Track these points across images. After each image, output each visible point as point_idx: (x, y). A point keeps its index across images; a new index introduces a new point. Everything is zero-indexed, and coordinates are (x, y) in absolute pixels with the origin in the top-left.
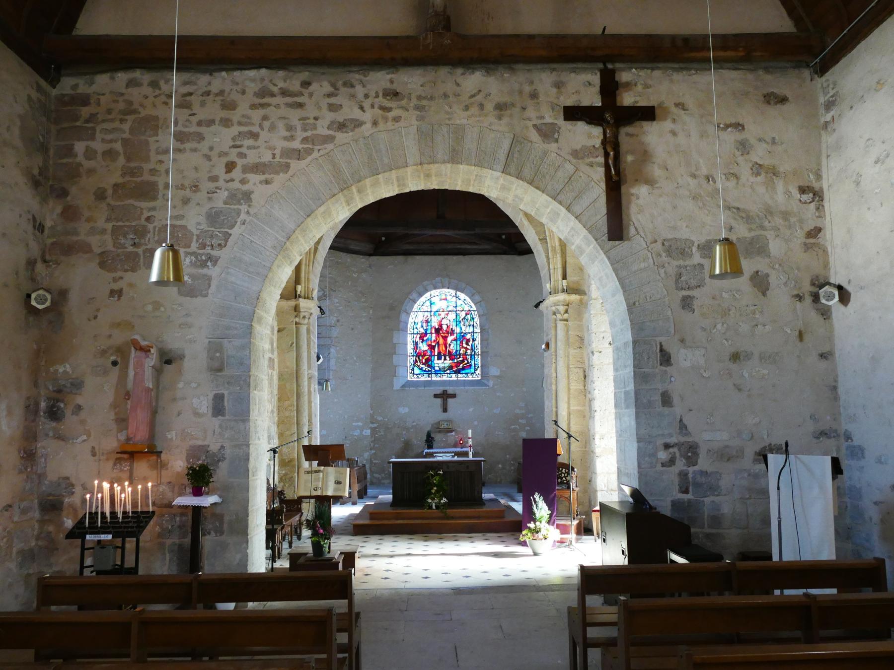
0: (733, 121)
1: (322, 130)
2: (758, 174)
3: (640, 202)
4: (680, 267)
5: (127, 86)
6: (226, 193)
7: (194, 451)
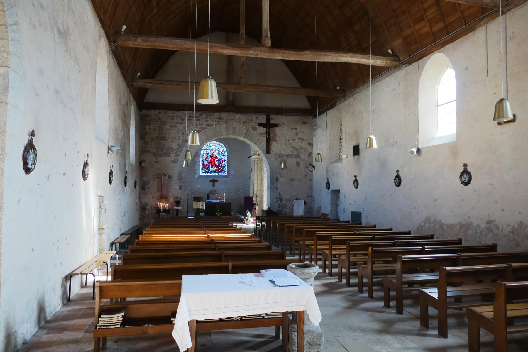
0: (295, 127)
1: (204, 126)
2: (299, 140)
3: (274, 145)
4: (281, 160)
5: (159, 113)
7: (175, 198)
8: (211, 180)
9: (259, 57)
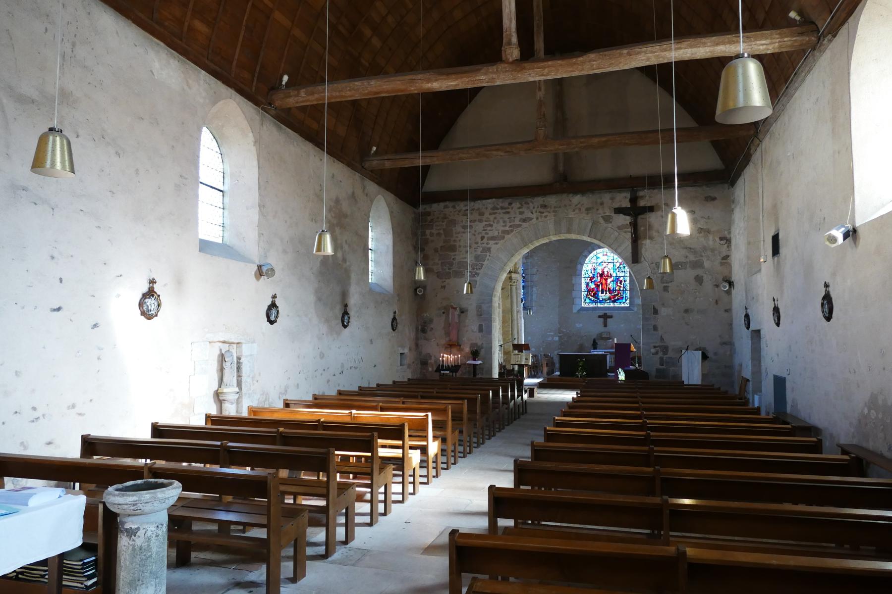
1: (517, 222)
2: (700, 233)
6: (481, 249)
7: (472, 345)
8: (601, 315)
9: (498, 83)
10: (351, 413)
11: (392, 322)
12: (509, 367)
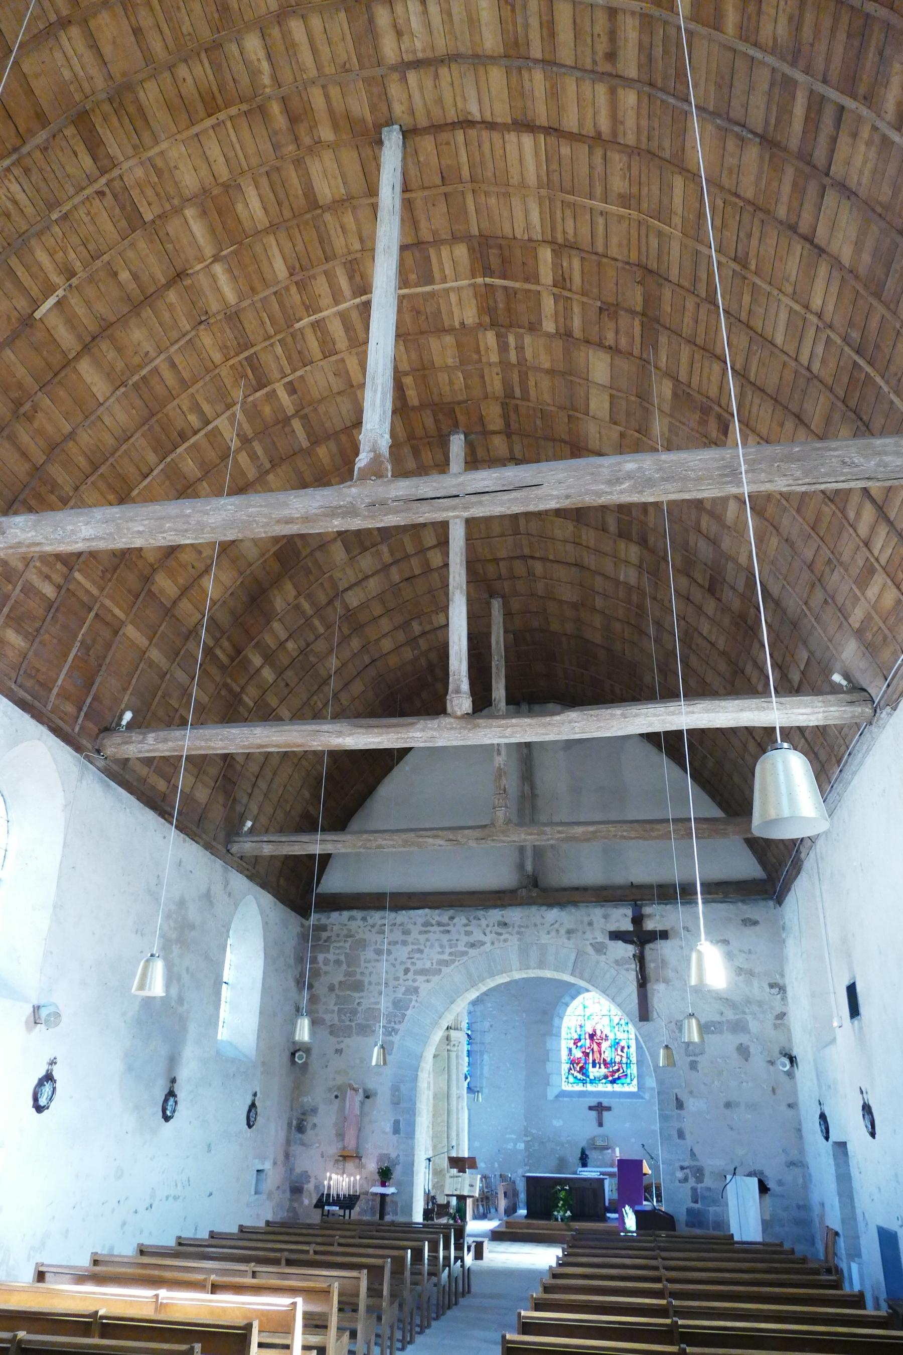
2: (740, 975)
3: (660, 995)
6: (404, 988)
7: (382, 1157)
8: (593, 1104)
10: (157, 1296)
11: (249, 1111)
12: (442, 1200)
